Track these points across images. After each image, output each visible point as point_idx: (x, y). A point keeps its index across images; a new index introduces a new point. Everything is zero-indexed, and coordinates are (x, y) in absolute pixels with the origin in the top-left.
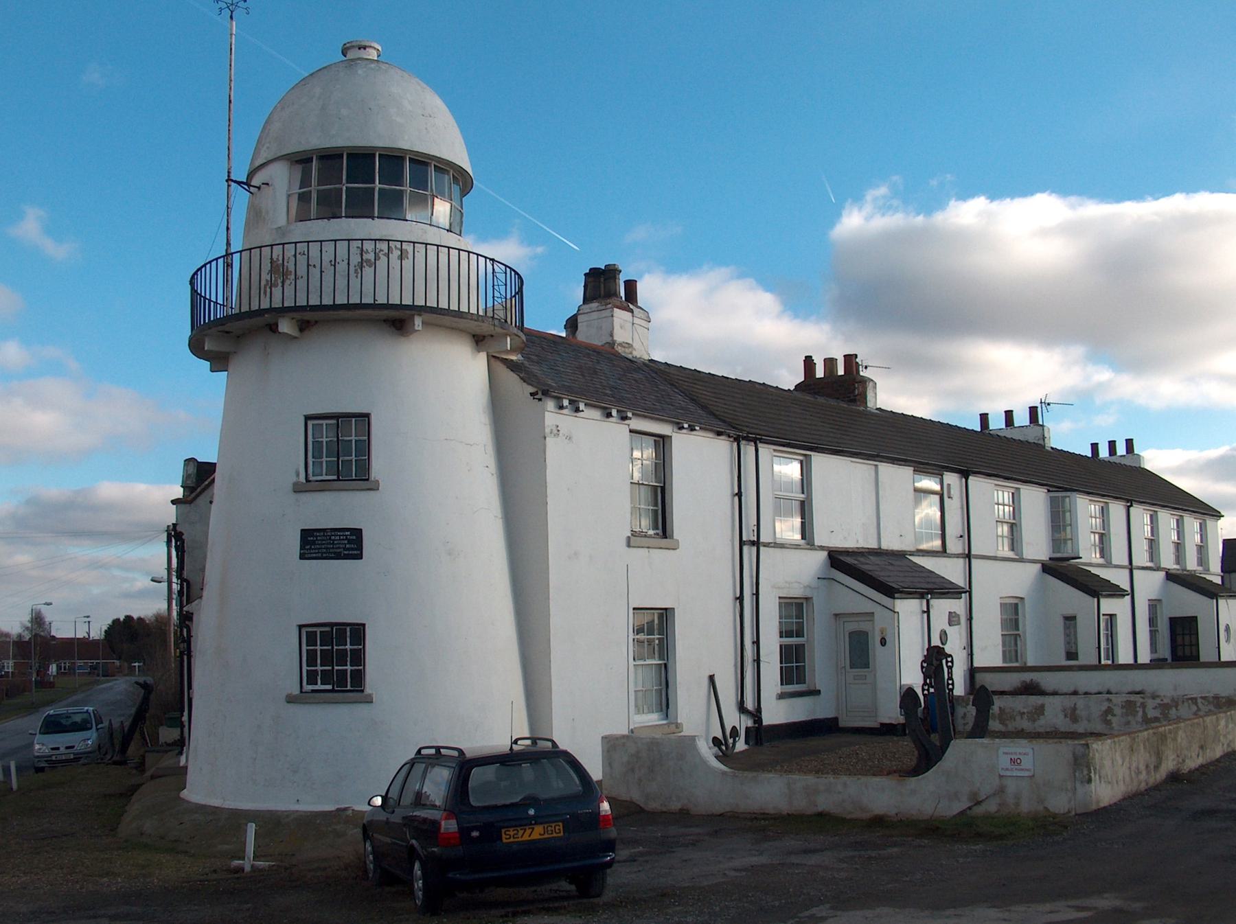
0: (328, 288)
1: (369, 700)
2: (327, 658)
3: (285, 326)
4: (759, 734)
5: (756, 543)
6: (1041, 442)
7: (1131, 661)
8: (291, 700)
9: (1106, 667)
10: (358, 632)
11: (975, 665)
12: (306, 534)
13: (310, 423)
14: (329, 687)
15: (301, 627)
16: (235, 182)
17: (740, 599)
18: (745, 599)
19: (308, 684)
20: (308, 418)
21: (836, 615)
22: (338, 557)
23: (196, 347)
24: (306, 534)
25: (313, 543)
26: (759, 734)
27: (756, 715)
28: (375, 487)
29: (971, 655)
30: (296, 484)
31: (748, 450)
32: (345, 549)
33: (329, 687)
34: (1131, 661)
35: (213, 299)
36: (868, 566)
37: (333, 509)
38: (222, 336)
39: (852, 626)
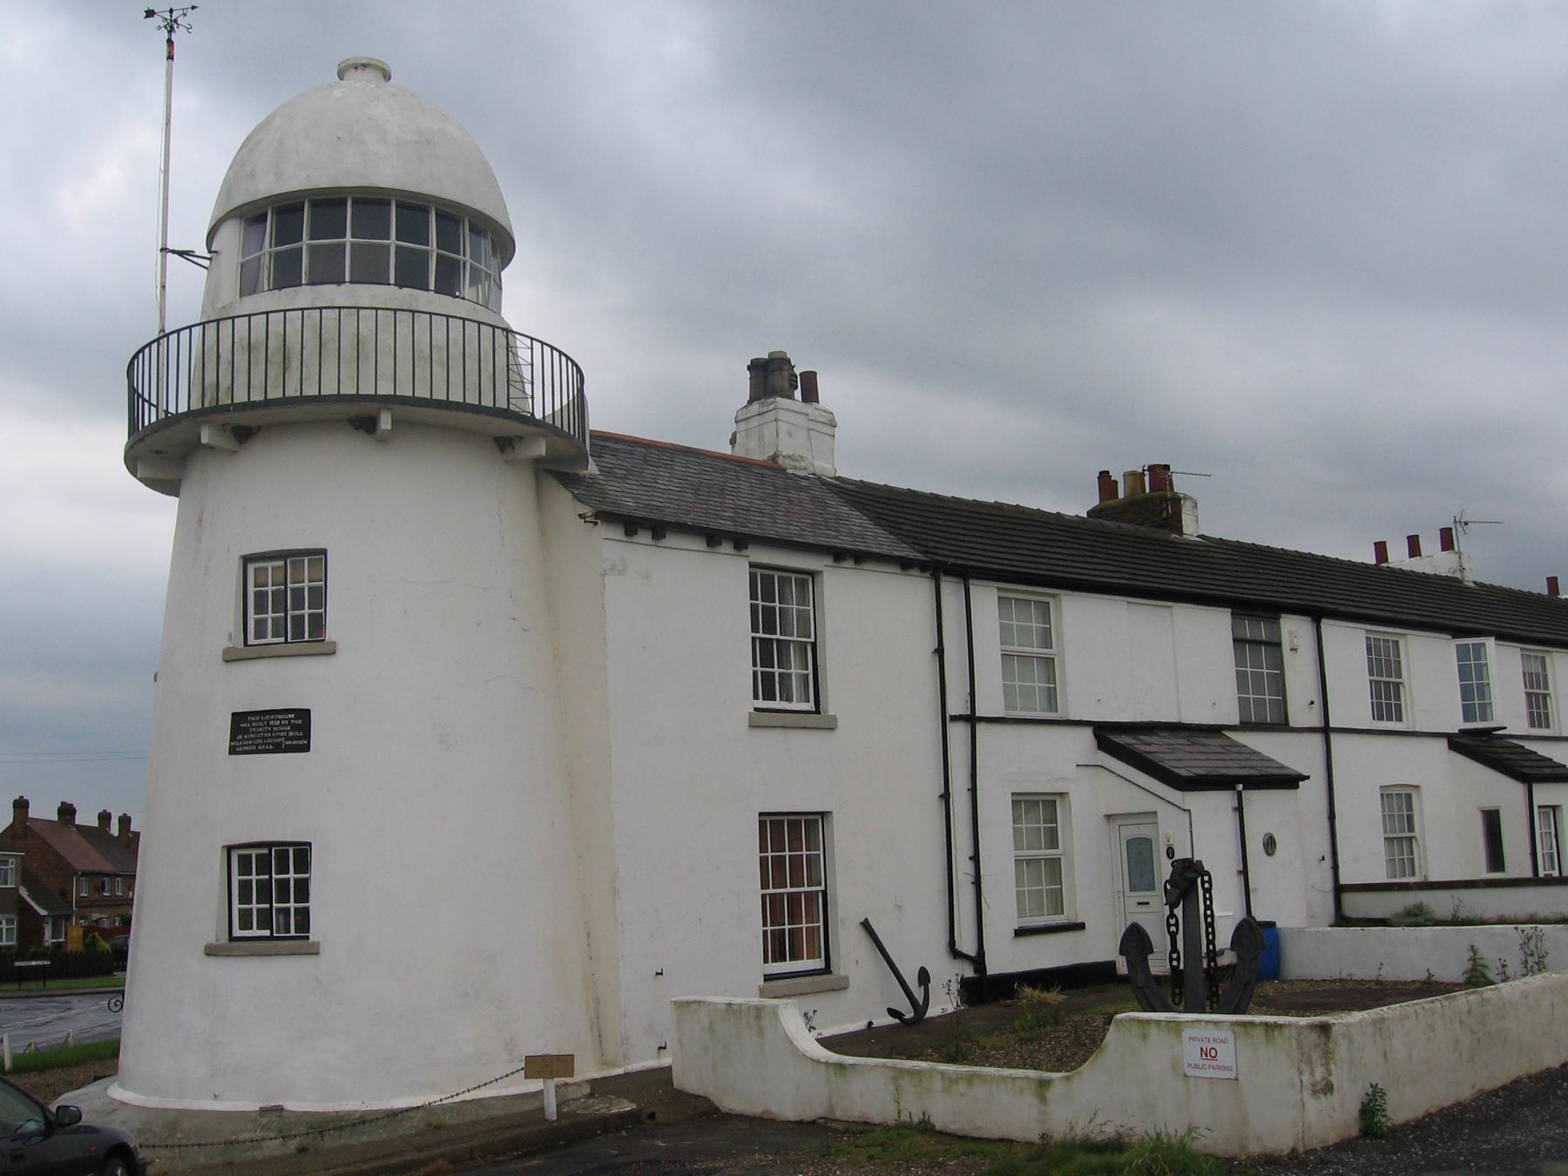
0: (456, 377)
1: (314, 951)
2: (264, 891)
3: (385, 422)
4: (983, 989)
5: (971, 719)
6: (1458, 575)
7: (1529, 874)
8: (212, 951)
9: (1549, 881)
10: (303, 853)
11: (1343, 880)
12: (238, 717)
13: (251, 568)
14: (267, 933)
15: (229, 849)
16: (174, 252)
17: (946, 797)
18: (955, 800)
19: (241, 928)
20: (247, 560)
21: (1109, 817)
22: (278, 749)
23: (133, 460)
24: (238, 717)
25: (246, 731)
26: (983, 989)
27: (978, 961)
28: (331, 652)
29: (1335, 867)
30: (226, 651)
31: (951, 590)
32: (287, 738)
33: (267, 933)
34: (1529, 874)
35: (154, 401)
36: (1153, 747)
37: (275, 684)
38: (164, 451)
39: (1131, 832)
